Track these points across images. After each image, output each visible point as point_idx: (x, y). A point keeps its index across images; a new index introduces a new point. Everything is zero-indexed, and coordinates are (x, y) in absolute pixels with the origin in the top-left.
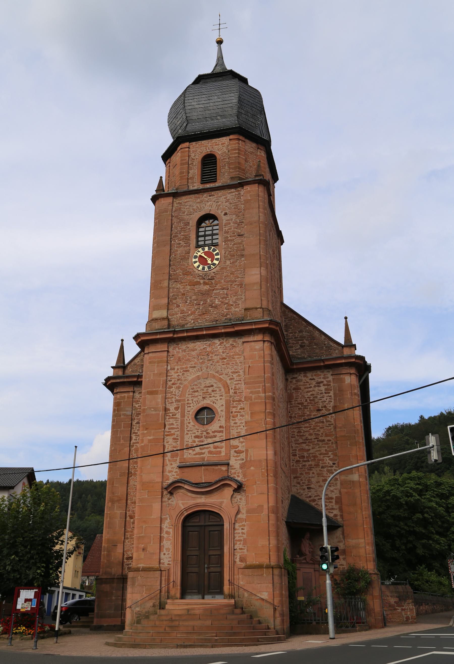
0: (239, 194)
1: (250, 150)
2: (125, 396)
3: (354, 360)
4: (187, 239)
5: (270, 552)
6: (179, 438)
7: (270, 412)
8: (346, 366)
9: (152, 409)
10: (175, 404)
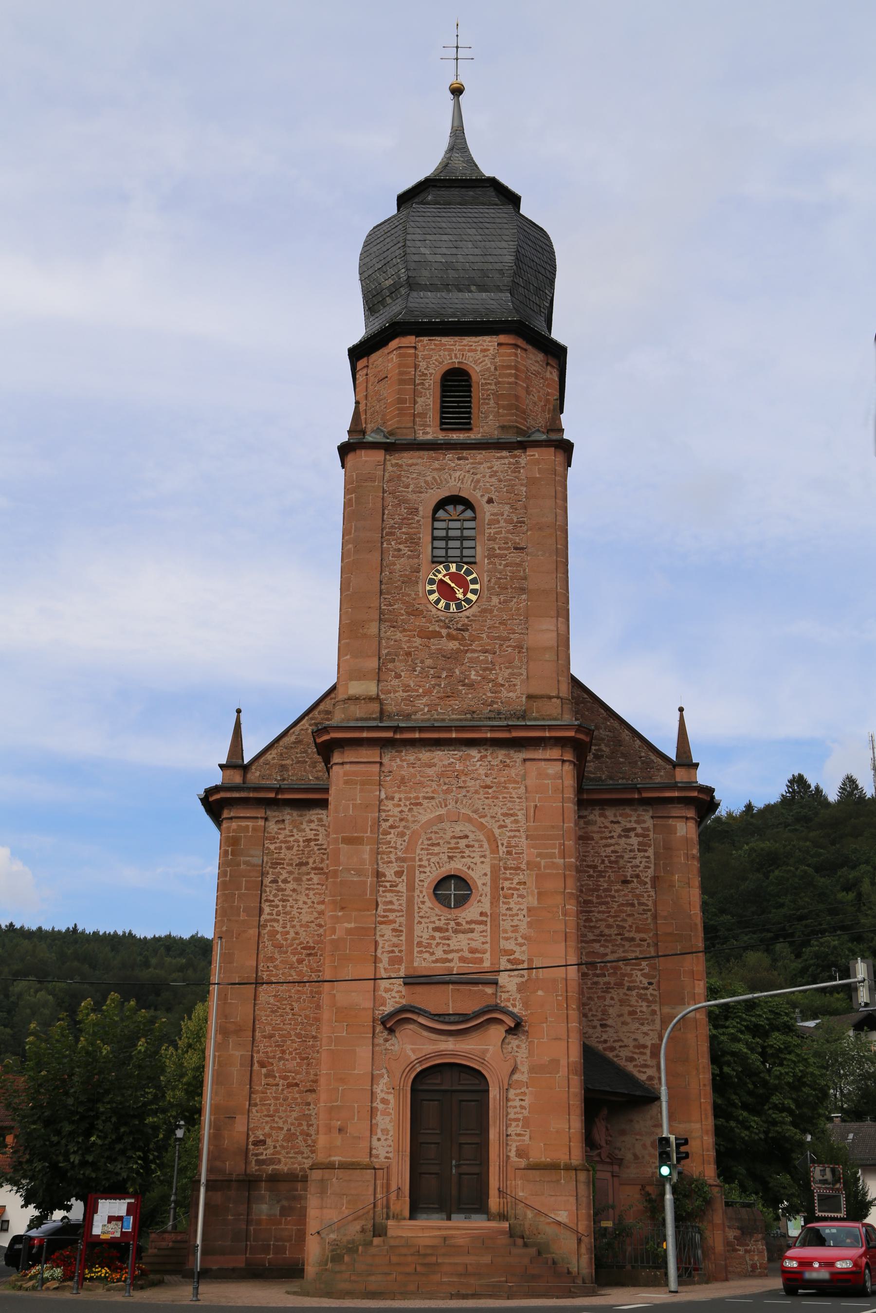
0: (517, 462)
1: (534, 368)
2: (248, 826)
3: (695, 794)
4: (413, 541)
5: (570, 1142)
6: (404, 929)
7: (572, 893)
8: (679, 803)
9: (352, 872)
10: (395, 864)
